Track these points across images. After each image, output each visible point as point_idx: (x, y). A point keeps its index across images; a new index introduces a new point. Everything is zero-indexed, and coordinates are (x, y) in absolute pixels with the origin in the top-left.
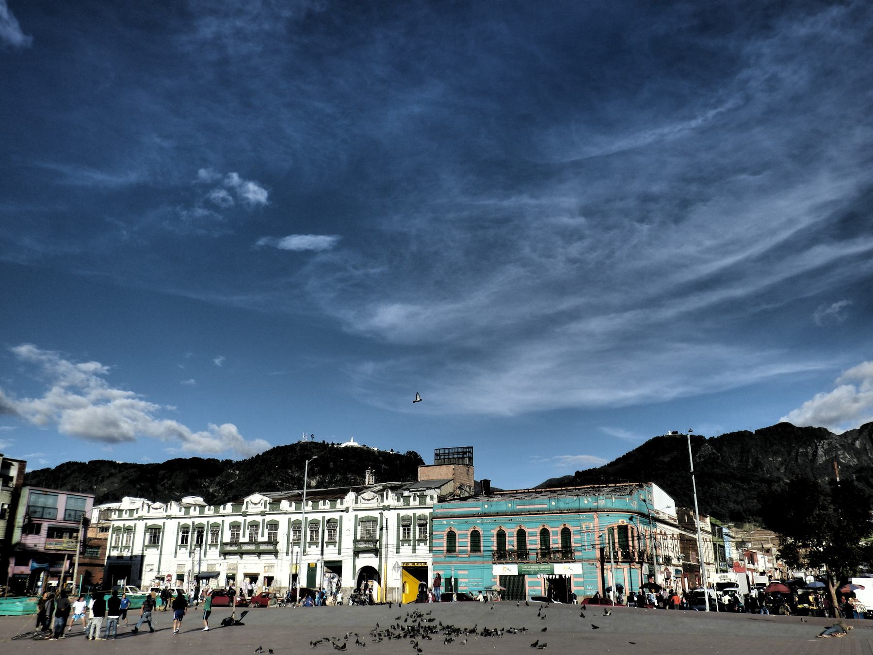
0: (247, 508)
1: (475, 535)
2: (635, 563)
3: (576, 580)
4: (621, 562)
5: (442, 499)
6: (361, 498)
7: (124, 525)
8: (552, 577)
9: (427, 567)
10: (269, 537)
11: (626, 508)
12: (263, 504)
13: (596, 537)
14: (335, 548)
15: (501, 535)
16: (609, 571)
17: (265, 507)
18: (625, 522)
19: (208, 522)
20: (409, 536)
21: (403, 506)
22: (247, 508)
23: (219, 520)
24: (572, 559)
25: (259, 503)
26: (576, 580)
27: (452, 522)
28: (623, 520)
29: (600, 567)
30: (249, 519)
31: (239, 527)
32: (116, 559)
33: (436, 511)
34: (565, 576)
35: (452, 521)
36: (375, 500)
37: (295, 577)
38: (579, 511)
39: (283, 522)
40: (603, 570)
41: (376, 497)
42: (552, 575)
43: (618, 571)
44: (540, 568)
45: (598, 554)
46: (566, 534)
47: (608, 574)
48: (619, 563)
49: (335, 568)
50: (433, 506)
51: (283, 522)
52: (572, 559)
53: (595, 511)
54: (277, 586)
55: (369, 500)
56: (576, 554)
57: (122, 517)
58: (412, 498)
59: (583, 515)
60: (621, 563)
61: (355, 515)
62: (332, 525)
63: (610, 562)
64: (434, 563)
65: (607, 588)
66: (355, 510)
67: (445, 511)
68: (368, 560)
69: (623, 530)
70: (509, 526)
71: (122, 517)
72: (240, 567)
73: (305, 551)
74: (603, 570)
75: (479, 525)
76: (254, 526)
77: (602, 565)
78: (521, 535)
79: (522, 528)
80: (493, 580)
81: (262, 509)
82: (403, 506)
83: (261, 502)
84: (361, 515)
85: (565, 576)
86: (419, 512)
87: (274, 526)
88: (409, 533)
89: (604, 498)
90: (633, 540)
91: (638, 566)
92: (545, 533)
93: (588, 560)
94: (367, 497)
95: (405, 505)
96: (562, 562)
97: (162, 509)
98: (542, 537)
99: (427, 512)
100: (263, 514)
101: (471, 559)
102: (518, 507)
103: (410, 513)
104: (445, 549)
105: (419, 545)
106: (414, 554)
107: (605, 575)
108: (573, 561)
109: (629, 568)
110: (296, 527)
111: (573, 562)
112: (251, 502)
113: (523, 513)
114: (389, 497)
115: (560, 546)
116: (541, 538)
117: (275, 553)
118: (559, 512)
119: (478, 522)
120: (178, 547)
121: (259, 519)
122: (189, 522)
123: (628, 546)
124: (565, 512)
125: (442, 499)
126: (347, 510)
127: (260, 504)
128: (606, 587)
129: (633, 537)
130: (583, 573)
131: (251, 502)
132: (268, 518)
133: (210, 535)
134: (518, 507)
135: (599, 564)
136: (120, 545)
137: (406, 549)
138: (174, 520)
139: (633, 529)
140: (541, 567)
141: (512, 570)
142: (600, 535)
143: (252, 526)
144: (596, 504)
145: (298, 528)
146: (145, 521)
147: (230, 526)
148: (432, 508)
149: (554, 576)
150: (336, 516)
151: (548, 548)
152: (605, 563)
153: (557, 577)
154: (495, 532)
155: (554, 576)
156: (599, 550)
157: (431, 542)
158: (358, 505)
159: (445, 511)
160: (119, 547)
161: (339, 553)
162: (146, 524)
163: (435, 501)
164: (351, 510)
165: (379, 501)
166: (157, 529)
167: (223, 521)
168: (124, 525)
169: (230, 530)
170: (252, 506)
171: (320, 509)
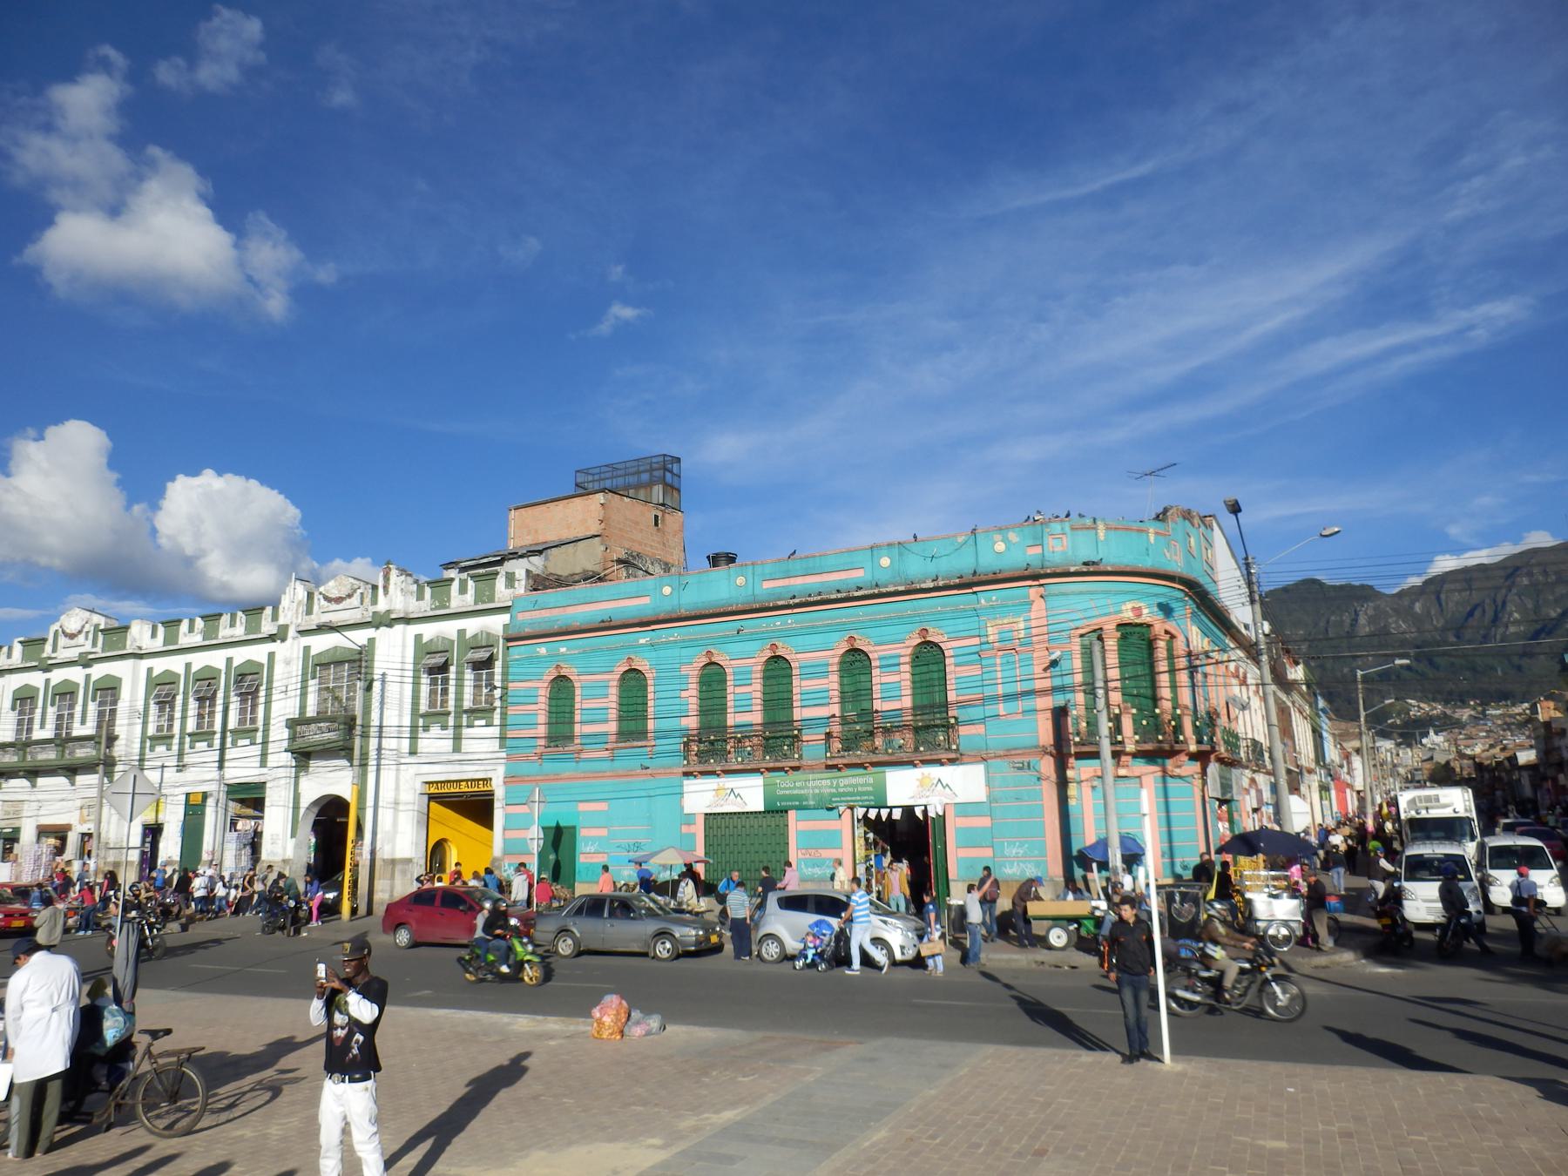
0: (54, 650)
1: (633, 681)
2: (1183, 758)
3: (962, 822)
4: (1135, 755)
5: (539, 583)
6: (321, 597)
7: (229, 660)
8: (879, 815)
9: (491, 794)
10: (58, 727)
11: (1147, 563)
12: (91, 636)
13: (1038, 670)
14: (169, 753)
15: (713, 679)
16: (1086, 788)
17: (94, 644)
18: (1145, 611)
19: (188, 666)
20: (444, 702)
21: (432, 609)
22: (54, 650)
23: (258, 653)
24: (949, 749)
25: (80, 632)
26: (962, 822)
27: (563, 650)
28: (1136, 605)
29: (1053, 777)
30: (57, 676)
31: (33, 698)
32: (313, 755)
33: (521, 617)
34: (925, 812)
35: (776, 621)
36: (355, 601)
37: (153, 832)
38: (969, 583)
39: (132, 678)
40: (1063, 783)
41: (359, 591)
42: (879, 808)
43: (1122, 784)
44: (837, 788)
45: (1045, 734)
46: (928, 657)
47: (1083, 800)
48: (1124, 758)
49: (250, 798)
50: (510, 604)
51: (132, 678)
52: (949, 749)
53: (1034, 576)
54: (109, 860)
55: (339, 600)
56: (963, 730)
57: (177, 643)
58: (455, 586)
59: (988, 597)
60: (1129, 758)
61: (416, 636)
62: (249, 683)
63: (1096, 755)
64: (510, 779)
65: (1080, 851)
66: (303, 633)
67: (545, 614)
68: (332, 780)
69: (1137, 639)
70: (735, 648)
71: (177, 643)
72: (27, 810)
73: (181, 755)
74: (1063, 783)
75: (643, 650)
76: (65, 694)
77: (1061, 767)
78: (777, 669)
79: (858, 645)
80: (684, 829)
81: (88, 647)
82: (432, 609)
83: (85, 630)
84: (321, 644)
85: (925, 812)
86: (472, 626)
87: (108, 691)
88: (445, 692)
89: (1067, 529)
90: (1172, 671)
91: (1195, 767)
92: (855, 662)
93: (1007, 754)
94: (334, 594)
95: (436, 608)
96: (912, 764)
97: (357, 596)
98: (846, 681)
99: (496, 624)
100: (86, 662)
101: (617, 764)
102: (767, 585)
103: (449, 629)
104: (542, 730)
105: (234, 744)
106: (457, 756)
107: (1072, 803)
108: (953, 756)
109: (1160, 774)
110: (162, 691)
111: (952, 761)
112: (64, 632)
113: (780, 603)
114: (391, 588)
115: (907, 702)
116: (841, 685)
117: (109, 764)
118: (901, 588)
119: (642, 641)
120: (188, 739)
121: (76, 674)
122: (176, 664)
123: (1155, 700)
124: (924, 586)
125: (539, 583)
126: (279, 636)
127: (83, 635)
128: (1075, 848)
129: (1171, 657)
130: (992, 799)
131: (64, 632)
132: (98, 671)
133: (193, 705)
134: (767, 585)
135: (1047, 766)
136: (218, 727)
137: (435, 741)
138: (399, 628)
139: (1173, 637)
140: (843, 782)
141: (749, 794)
142: (1053, 657)
143: (63, 695)
144: (1038, 550)
145: (167, 695)
146: (145, 664)
147: (15, 700)
148: (505, 609)
149: (884, 813)
150: (258, 653)
151: (868, 715)
152: (1072, 761)
153: (897, 814)
154: (692, 672)
155: (884, 813)
156: (1049, 715)
157: (504, 715)
158: (313, 617)
159: (545, 614)
160: (172, 737)
161: (263, 764)
162: (307, 649)
163: (521, 587)
164: (292, 632)
165: (367, 600)
166: (67, 693)
167: (271, 656)
168: (229, 660)
169: (13, 708)
170: (62, 641)
171: (223, 637)
